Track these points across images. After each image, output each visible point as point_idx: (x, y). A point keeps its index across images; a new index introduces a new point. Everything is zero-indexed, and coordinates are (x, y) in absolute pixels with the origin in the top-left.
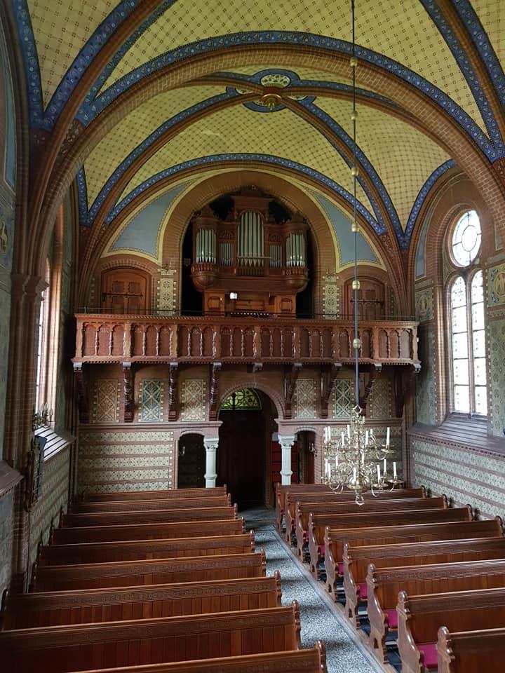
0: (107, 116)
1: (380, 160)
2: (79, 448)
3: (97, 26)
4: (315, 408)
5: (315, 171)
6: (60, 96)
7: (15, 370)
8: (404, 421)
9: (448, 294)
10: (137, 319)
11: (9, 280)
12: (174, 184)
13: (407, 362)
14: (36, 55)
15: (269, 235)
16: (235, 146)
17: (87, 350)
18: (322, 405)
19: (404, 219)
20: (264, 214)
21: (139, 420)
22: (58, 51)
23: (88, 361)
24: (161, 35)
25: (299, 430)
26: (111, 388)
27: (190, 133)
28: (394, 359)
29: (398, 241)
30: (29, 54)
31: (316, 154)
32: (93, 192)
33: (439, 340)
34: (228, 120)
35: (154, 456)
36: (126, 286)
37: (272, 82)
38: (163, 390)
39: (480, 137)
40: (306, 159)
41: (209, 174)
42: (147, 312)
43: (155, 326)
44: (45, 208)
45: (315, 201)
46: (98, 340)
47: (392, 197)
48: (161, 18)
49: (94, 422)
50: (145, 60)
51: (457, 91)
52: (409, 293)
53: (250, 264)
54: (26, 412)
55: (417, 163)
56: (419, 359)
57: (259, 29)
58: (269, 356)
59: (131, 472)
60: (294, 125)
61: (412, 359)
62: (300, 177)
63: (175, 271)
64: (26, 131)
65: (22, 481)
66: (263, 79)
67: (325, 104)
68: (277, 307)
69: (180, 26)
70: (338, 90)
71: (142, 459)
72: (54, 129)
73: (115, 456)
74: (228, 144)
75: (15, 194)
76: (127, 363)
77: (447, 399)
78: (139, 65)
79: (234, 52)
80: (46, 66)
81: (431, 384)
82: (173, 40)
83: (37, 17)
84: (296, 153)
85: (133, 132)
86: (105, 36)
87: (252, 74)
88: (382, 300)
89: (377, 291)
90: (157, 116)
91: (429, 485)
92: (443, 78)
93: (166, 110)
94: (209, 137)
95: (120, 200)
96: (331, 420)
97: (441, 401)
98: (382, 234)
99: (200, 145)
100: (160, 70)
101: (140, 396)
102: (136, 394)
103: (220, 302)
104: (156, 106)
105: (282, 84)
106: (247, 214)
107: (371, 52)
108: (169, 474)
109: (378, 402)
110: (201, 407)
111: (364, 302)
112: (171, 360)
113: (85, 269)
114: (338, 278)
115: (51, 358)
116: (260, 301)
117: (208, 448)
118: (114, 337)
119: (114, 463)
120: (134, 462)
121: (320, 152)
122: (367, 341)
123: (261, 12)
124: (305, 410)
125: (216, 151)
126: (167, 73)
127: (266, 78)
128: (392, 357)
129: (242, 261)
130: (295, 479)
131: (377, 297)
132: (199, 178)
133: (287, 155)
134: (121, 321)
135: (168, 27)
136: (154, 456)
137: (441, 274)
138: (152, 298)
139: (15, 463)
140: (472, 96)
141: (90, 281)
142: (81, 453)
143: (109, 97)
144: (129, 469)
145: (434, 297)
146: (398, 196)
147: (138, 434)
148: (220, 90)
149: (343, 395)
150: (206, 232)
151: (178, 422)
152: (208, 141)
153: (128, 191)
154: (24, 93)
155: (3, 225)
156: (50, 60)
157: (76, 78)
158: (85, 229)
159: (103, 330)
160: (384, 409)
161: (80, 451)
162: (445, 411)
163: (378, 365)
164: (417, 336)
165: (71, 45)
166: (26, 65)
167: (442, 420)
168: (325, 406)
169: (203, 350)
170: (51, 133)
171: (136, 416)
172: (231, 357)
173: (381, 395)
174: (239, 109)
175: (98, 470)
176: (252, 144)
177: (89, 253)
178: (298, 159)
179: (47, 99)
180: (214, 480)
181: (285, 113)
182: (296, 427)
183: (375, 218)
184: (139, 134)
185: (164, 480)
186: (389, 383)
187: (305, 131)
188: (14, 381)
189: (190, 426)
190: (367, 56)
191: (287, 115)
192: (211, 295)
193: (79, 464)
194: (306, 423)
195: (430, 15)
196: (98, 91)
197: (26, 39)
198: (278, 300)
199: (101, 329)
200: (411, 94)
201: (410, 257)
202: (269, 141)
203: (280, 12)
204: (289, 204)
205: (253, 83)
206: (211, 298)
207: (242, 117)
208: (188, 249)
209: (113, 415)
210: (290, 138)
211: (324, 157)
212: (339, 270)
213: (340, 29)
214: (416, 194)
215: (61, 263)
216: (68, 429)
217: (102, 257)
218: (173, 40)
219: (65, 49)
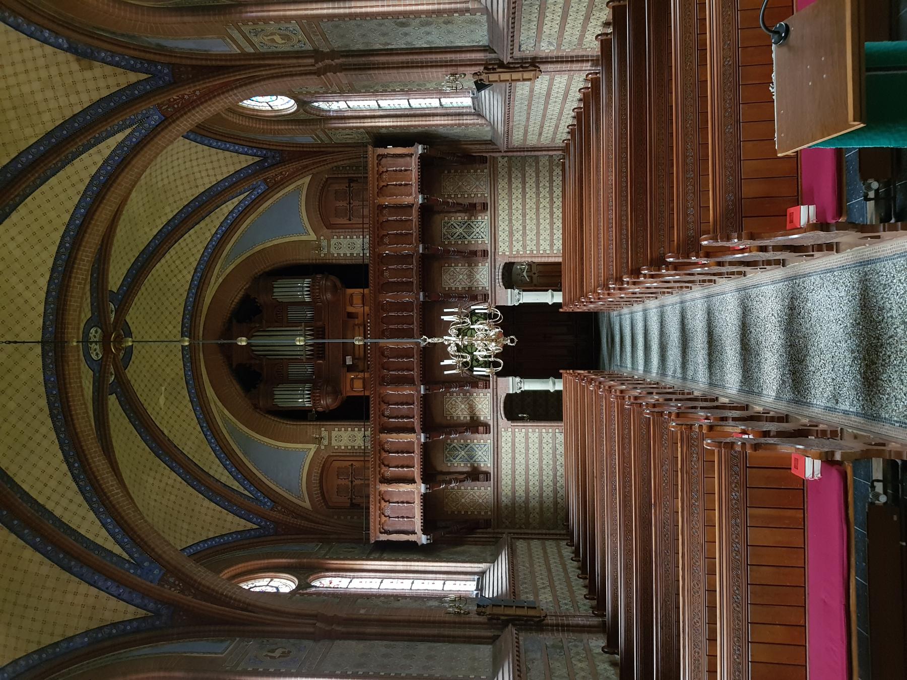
1: (177, 199)
3: (64, 571)
4: (476, 265)
6: (138, 601)
8: (492, 154)
10: (375, 478)
12: (225, 432)
14: (100, 629)
15: (276, 322)
16: (176, 368)
17: (410, 528)
18: (472, 256)
19: (246, 161)
21: (489, 465)
22: (94, 608)
23: (420, 528)
24: (64, 502)
25: (501, 284)
26: (454, 496)
29: (272, 166)
31: (176, 271)
32: (239, 524)
33: (388, 124)
35: (527, 448)
36: (343, 482)
37: (97, 347)
38: (456, 441)
41: (210, 392)
42: (366, 459)
45: (232, 267)
46: (398, 517)
47: (220, 178)
49: (489, 513)
51: (86, 168)
53: (312, 348)
54: (449, 623)
55: (175, 157)
56: (412, 145)
63: (323, 429)
65: (514, 625)
67: (115, 279)
70: (98, 274)
74: (173, 375)
75: (238, 639)
76: (422, 488)
77: (459, 114)
78: (98, 522)
80: (109, 617)
81: (441, 130)
82: (68, 488)
83: (64, 632)
86: (73, 563)
87: (91, 373)
89: (336, 187)
91: (562, 133)
92: (73, 185)
93: (141, 456)
94: (167, 399)
95: (246, 493)
96: (489, 245)
97: (461, 122)
98: (267, 184)
101: (462, 465)
102: (460, 469)
103: (356, 378)
104: (137, 469)
106: (253, 348)
109: (469, 187)
110: (475, 398)
111: (350, 203)
114: (322, 238)
115: (416, 568)
116: (354, 329)
117: (520, 388)
118: (395, 500)
120: (534, 470)
121: (173, 267)
124: (478, 277)
127: (94, 356)
128: (411, 180)
129: (309, 353)
130: (557, 287)
131: (343, 186)
132: (215, 404)
133: (180, 304)
134: (377, 494)
137: (310, 121)
138: (352, 454)
139: (496, 633)
140: (91, 151)
142: (523, 526)
143: (134, 550)
144: (541, 475)
147: (504, 466)
149: (461, 230)
151: (491, 423)
153: (235, 485)
156: (103, 614)
159: (388, 512)
160: (477, 179)
161: (520, 528)
162: (472, 117)
164: (386, 147)
165: (86, 595)
167: (483, 122)
168: (474, 253)
169: (407, 404)
171: (484, 469)
172: (415, 373)
173: (460, 184)
179: (142, 613)
181: (131, 319)
182: (498, 288)
183: (246, 194)
185: (554, 438)
186: (446, 172)
188: (419, 635)
189: (495, 410)
191: (133, 317)
192: (348, 388)
193: (534, 528)
194: (493, 276)
195: (6, 218)
197: (86, 639)
198: (350, 309)
199: (386, 514)
203: (24, 377)
208: (299, 415)
209: (482, 494)
211: (178, 262)
212: (313, 237)
213: (33, 309)
216: (497, 542)
217: (310, 508)
218: (68, 488)
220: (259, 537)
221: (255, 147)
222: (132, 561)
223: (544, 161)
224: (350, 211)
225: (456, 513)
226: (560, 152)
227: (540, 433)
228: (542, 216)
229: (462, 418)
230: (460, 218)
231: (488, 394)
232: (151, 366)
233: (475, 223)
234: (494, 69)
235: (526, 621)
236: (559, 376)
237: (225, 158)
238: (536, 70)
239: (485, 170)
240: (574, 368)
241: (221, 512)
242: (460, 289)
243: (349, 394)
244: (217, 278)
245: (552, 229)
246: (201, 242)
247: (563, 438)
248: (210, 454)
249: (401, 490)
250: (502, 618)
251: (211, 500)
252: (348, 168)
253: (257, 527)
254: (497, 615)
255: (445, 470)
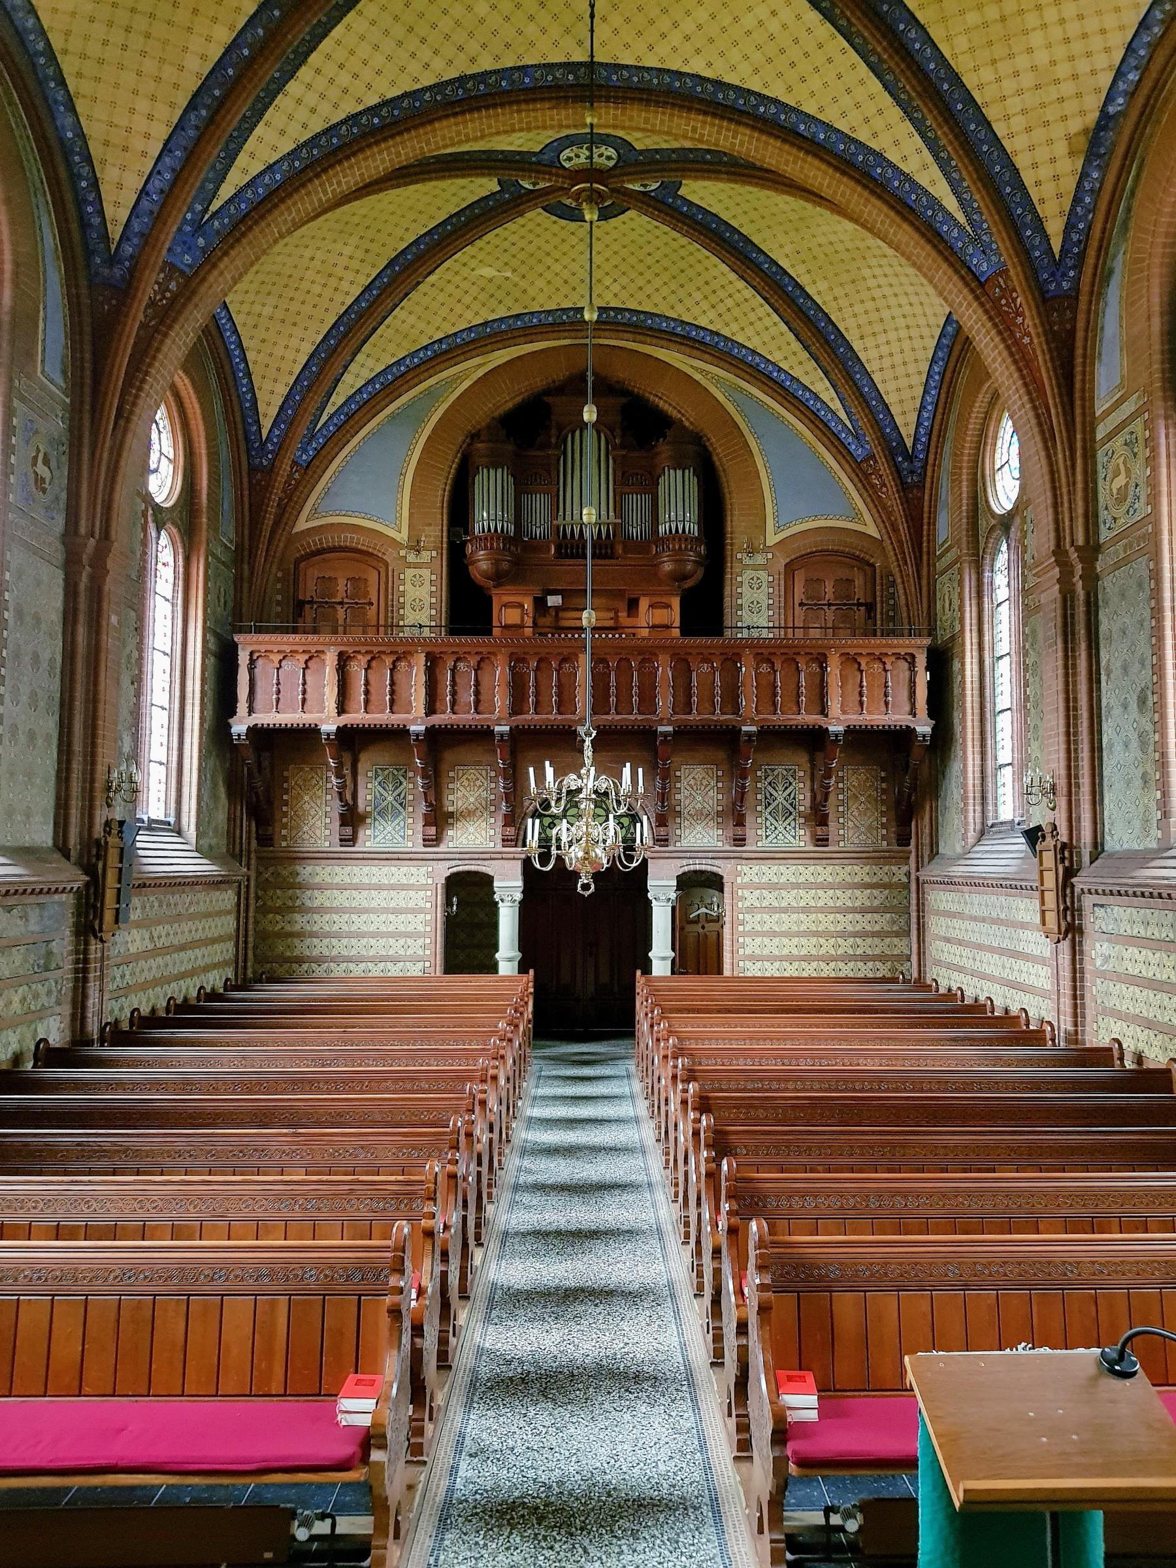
0: (226, 253)
1: (840, 301)
2: (256, 893)
5: (717, 334)
6: (136, 226)
7: (72, 699)
9: (987, 574)
11: (60, 547)
13: (904, 724)
14: (88, 159)
17: (258, 704)
19: (906, 424)
20: (612, 431)
21: (368, 844)
22: (125, 149)
23: (259, 722)
24: (311, 99)
25: (686, 869)
27: (449, 275)
28: (876, 717)
30: (77, 159)
32: (269, 404)
34: (522, 244)
35: (396, 911)
37: (582, 160)
39: (955, 233)
40: (696, 311)
41: (502, 356)
43: (383, 657)
44: (122, 422)
47: (876, 377)
48: (303, 69)
49: (284, 844)
50: (287, 146)
51: (896, 143)
52: (924, 582)
55: (914, 299)
56: (931, 715)
57: (498, 66)
58: (608, 714)
59: (354, 941)
60: (657, 243)
61: (915, 715)
62: (688, 350)
64: (84, 291)
66: (563, 155)
68: (647, 616)
69: (344, 79)
71: (373, 917)
72: (130, 284)
73: (321, 910)
74: (532, 292)
75: (68, 400)
79: (455, 114)
80: (108, 176)
81: (955, 767)
82: (336, 106)
83: (84, 97)
84: (672, 299)
85: (333, 282)
87: (538, 150)
88: (869, 600)
89: (859, 582)
90: (374, 247)
91: (949, 979)
93: (390, 235)
94: (491, 280)
95: (324, 418)
98: (866, 460)
99: (475, 298)
100: (318, 161)
101: (369, 797)
105: (603, 160)
106: (578, 433)
107: (719, 84)
108: (424, 947)
109: (856, 813)
112: (414, 721)
113: (261, 553)
115: (188, 714)
116: (609, 610)
117: (502, 900)
118: (308, 678)
119: (321, 923)
120: (359, 923)
122: (818, 681)
123: (495, 33)
124: (699, 828)
125: (509, 309)
126: (332, 166)
127: (566, 153)
128: (869, 713)
130: (679, 967)
132: (480, 366)
134: (320, 648)
135: (320, 83)
136: (396, 911)
140: (926, 152)
141: (272, 577)
142: (260, 903)
144: (350, 935)
145: (961, 583)
146: (888, 374)
147: (366, 869)
148: (488, 185)
149: (780, 799)
150: (492, 472)
151: (442, 848)
152: (491, 289)
153: (338, 399)
154: (74, 226)
155: (38, 450)
157: (162, 191)
158: (259, 476)
161: (257, 898)
162: (978, 821)
163: (836, 728)
164: (927, 669)
165: (147, 136)
166: (74, 178)
167: (971, 841)
170: (126, 290)
173: (863, 799)
174: (539, 219)
175: (292, 935)
176: (565, 290)
177: (270, 520)
178: (679, 312)
179: (115, 232)
180: (516, 963)
184: (345, 286)
185: (415, 960)
186: (883, 774)
187: (683, 252)
189: (464, 855)
190: (714, 93)
191: (634, 221)
192: (506, 599)
193: (257, 922)
194: (700, 855)
196: (206, 210)
199: (283, 663)
200: (810, 159)
201: (926, 504)
202: (615, 281)
204: (666, 407)
205: (546, 165)
206: (506, 605)
207: (548, 235)
209: (318, 832)
210: (657, 268)
212: (772, 539)
213: (651, 48)
214: (925, 367)
215: (204, 539)
216: (233, 856)
218: (336, 106)
219: (138, 144)
220: (247, 439)
221: (930, 440)
222: (207, 217)
223: (900, 946)
224: (815, 605)
225: (285, 785)
226: (915, 975)
227: (423, 935)
228: (804, 941)
229: (451, 797)
230: (802, 797)
231: (492, 844)
232: (548, 254)
233: (793, 824)
234: (1063, 860)
235: (94, 907)
236: (523, 968)
237: (911, 387)
238: (1060, 933)
239: (885, 843)
240: (536, 995)
241: (291, 373)
242: (678, 797)
243: (495, 600)
244: (702, 371)
245: (781, 959)
246: (764, 343)
247: (415, 974)
248: (393, 355)
249: (327, 690)
250: (100, 865)
251: (312, 356)
252: (892, 602)
253: (264, 438)
254: (106, 855)
255: (361, 767)
